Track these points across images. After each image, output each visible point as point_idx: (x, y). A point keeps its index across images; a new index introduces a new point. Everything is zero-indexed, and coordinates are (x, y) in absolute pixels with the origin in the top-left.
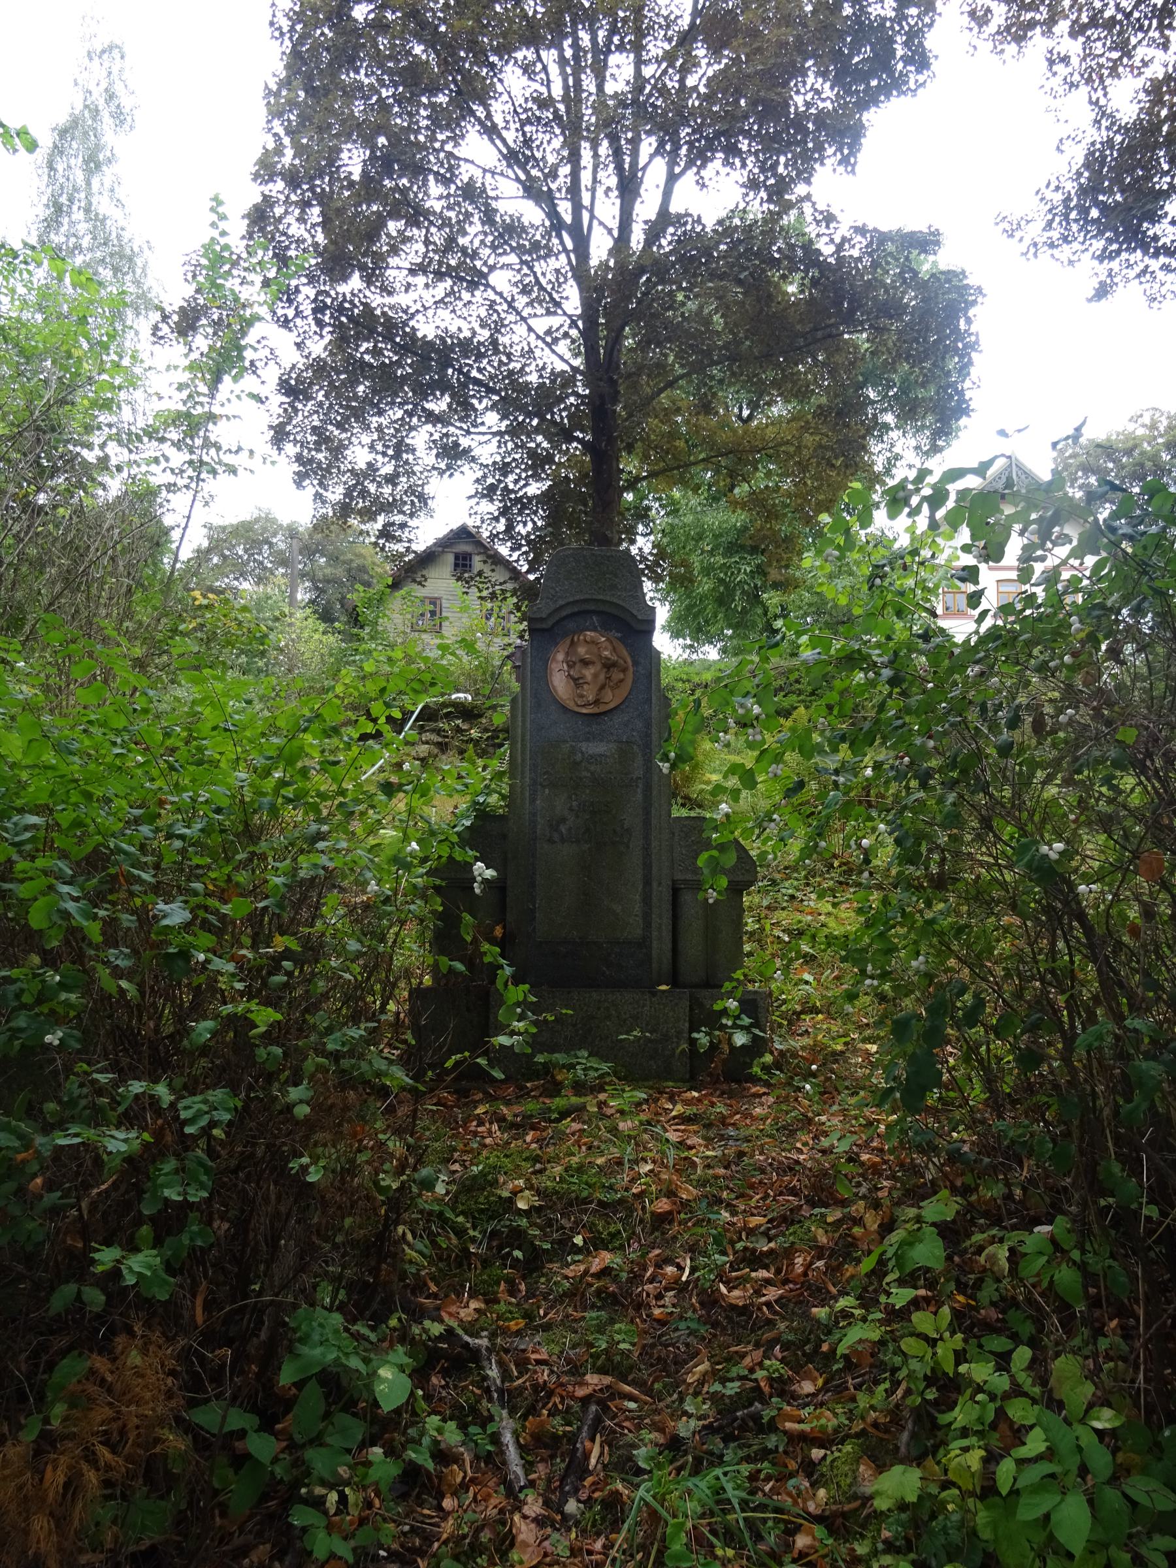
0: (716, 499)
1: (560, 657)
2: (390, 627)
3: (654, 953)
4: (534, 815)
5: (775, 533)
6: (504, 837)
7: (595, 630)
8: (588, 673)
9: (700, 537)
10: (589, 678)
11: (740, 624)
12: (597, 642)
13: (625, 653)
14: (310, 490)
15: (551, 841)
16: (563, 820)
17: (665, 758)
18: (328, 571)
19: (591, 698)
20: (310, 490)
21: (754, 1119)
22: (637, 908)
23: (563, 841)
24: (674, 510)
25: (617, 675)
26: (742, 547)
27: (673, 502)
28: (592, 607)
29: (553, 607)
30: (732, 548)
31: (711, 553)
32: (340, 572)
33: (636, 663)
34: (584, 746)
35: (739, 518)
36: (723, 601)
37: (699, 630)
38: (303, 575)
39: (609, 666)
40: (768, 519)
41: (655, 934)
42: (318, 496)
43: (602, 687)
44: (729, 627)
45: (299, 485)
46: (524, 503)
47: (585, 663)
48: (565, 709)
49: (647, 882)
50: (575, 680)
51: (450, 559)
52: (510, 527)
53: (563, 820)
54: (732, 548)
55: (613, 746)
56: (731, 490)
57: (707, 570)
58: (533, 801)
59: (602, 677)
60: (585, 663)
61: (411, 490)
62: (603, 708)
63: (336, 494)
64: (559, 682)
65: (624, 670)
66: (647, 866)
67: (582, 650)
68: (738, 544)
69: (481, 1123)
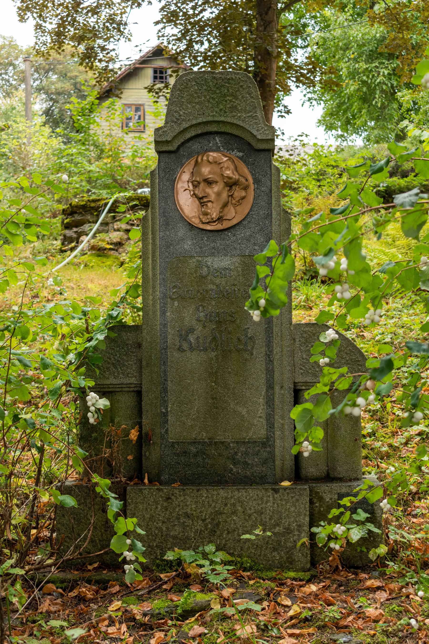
0: (360, 15)
1: (186, 177)
2: (99, 132)
3: (278, 452)
4: (165, 325)
5: (405, 41)
6: (139, 346)
7: (217, 150)
8: (212, 192)
9: (346, 48)
10: (213, 197)
11: (380, 116)
12: (219, 162)
13: (246, 171)
14: (31, 22)
15: (180, 349)
16: (191, 330)
17: (256, 306)
18: (59, 85)
19: (215, 216)
20: (31, 21)
21: (366, 619)
22: (261, 410)
23: (192, 349)
24: (326, 25)
25: (238, 193)
26: (381, 54)
27: (325, 20)
28: (213, 128)
29: (178, 130)
30: (373, 56)
31: (356, 60)
32: (67, 86)
33: (257, 181)
34: (209, 260)
35: (378, 30)
36: (366, 99)
37: (348, 122)
38: (39, 90)
39: (231, 184)
40: (400, 30)
41: (278, 433)
42: (38, 27)
43: (225, 205)
44: (372, 119)
45: (22, 19)
46: (201, 27)
47: (209, 182)
48: (191, 227)
49: (270, 387)
50: (200, 199)
51: (149, 73)
52: (190, 45)
53: (191, 330)
54: (373, 56)
55: (236, 260)
56: (372, 7)
57: (352, 75)
58: (164, 313)
59: (225, 195)
60: (209, 182)
61: (111, 19)
62: (226, 225)
63: (51, 25)
64: (186, 202)
65: (246, 188)
66: (270, 372)
67: (206, 170)
68: (379, 52)
69: (112, 622)
